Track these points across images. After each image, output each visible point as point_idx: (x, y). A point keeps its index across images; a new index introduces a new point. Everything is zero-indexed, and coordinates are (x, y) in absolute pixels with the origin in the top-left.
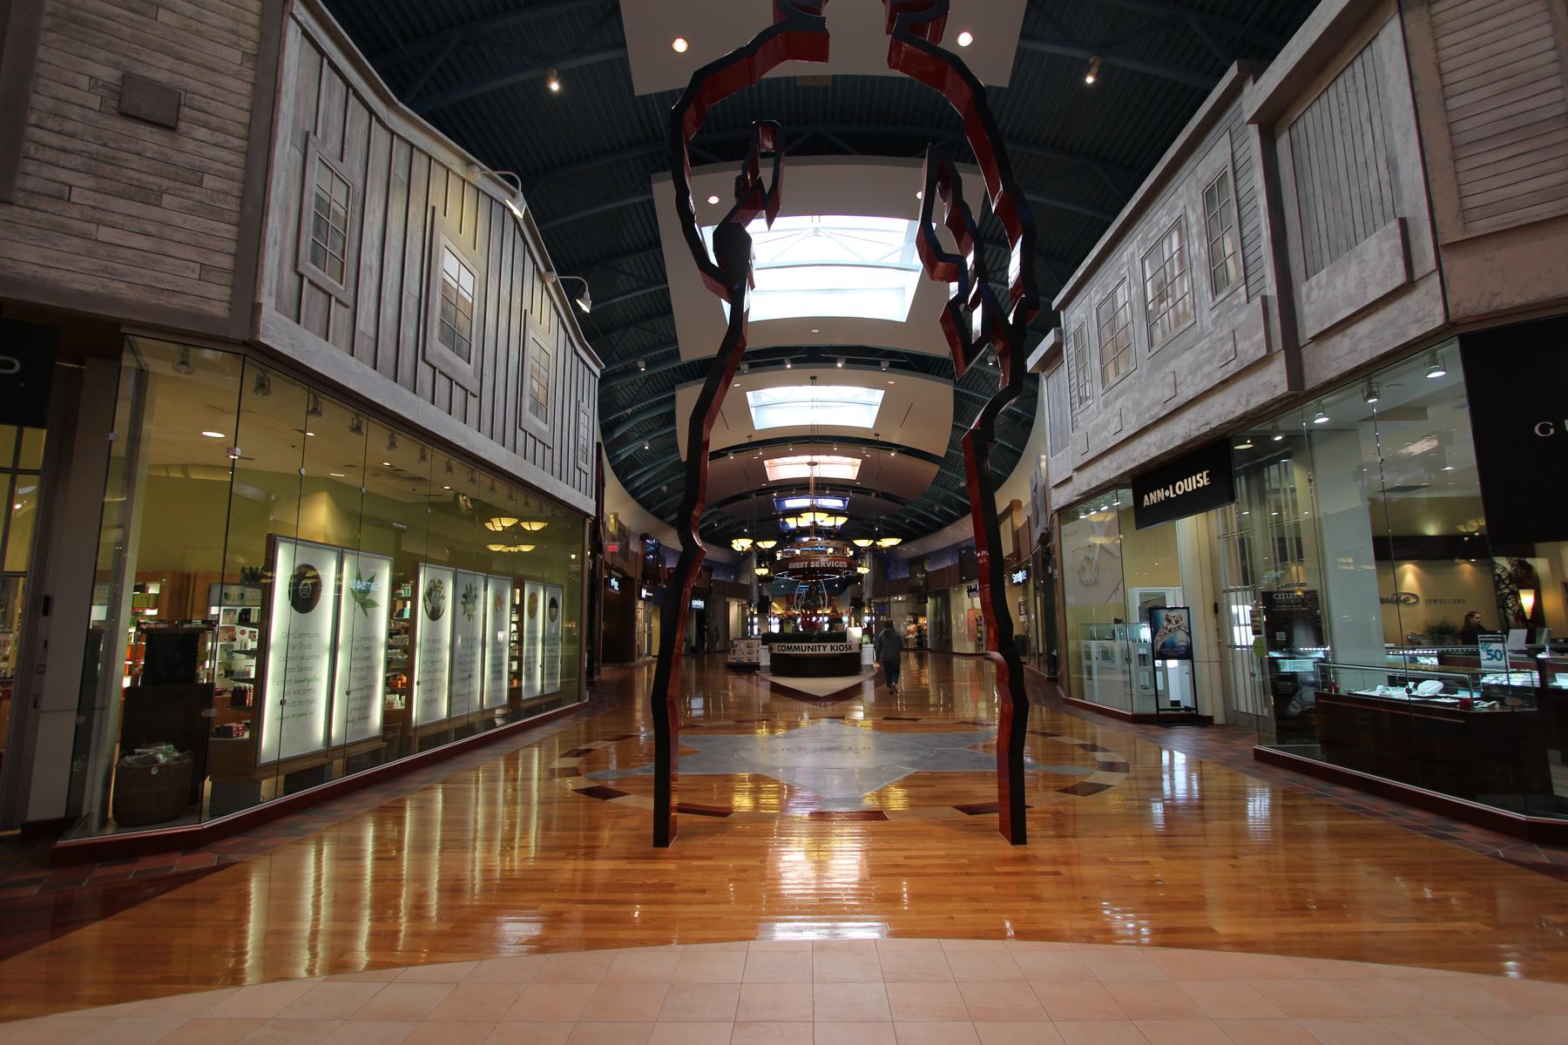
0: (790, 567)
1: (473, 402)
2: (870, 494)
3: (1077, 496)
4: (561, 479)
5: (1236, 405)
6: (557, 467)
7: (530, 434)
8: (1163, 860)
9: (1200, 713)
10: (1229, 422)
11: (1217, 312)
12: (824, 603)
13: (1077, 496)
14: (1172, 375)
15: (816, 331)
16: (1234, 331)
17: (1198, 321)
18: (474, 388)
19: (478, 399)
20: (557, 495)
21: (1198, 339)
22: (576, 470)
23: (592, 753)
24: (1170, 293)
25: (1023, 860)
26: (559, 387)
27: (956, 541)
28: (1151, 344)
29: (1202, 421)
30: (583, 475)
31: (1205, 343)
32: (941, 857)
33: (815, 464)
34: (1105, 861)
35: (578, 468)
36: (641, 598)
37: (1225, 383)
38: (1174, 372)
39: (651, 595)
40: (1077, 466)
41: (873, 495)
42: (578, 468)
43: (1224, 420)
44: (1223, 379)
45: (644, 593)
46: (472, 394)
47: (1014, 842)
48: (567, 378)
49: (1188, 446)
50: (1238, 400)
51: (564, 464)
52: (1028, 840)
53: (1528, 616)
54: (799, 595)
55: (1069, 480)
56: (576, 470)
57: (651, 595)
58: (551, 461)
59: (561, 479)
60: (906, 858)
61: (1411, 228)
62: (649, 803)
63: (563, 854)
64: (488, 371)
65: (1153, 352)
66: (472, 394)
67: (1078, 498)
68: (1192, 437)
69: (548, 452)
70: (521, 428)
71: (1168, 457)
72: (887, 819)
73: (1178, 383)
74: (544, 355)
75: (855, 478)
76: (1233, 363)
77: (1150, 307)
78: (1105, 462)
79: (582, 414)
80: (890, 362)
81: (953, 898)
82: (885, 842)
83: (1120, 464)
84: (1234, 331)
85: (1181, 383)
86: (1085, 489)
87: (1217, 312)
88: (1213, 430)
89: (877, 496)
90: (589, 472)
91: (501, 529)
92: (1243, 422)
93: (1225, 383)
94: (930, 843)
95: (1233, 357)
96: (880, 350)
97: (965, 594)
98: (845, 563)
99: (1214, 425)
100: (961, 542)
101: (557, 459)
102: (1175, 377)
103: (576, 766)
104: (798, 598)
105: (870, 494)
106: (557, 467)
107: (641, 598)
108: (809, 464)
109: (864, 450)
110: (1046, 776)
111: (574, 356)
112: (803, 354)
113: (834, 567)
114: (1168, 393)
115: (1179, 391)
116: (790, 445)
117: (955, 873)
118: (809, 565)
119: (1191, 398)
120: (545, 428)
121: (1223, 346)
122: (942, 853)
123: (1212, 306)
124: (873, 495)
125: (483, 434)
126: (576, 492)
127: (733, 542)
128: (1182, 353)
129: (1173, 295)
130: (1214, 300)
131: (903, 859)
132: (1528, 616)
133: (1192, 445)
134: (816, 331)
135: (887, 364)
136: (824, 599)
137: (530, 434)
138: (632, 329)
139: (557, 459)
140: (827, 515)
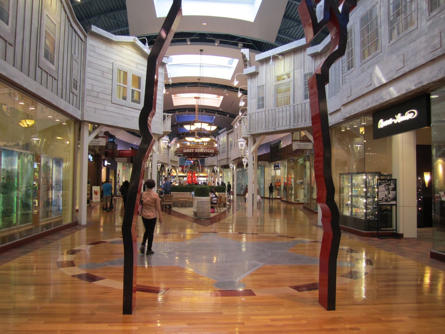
0: (184, 151)
1: (10, 49)
2: (226, 115)
3: (343, 119)
4: (62, 98)
5: (438, 73)
6: (60, 91)
7: (44, 71)
8: (409, 319)
9: (398, 232)
10: (433, 82)
11: (431, 22)
12: (200, 170)
13: (343, 119)
14: (402, 56)
15: (205, 24)
16: (441, 33)
17: (419, 26)
18: (11, 40)
19: (13, 47)
20: (60, 107)
21: (418, 37)
22: (71, 93)
23: (82, 252)
24: (403, 11)
25: (333, 321)
26: (62, 45)
27: (269, 141)
28: (391, 38)
29: (418, 81)
30: (75, 97)
31: (423, 39)
32: (291, 319)
33: (199, 98)
34: (379, 320)
35: (72, 92)
36: (104, 166)
37: (433, 61)
38: (403, 54)
39: (110, 164)
40: (344, 104)
41: (228, 116)
42: (72, 92)
43: (430, 81)
44: (432, 59)
45: (106, 163)
46: (10, 44)
47: (329, 309)
48: (66, 40)
49: (406, 95)
50: (439, 70)
51: (64, 90)
52: (336, 307)
53: (427, 186)
54: (187, 166)
55: (339, 110)
56: (71, 93)
57: (110, 164)
58: (56, 87)
59: (62, 98)
60: (272, 320)
61: (236, 92)
62: (119, 285)
63: (68, 319)
64: (19, 31)
65: (391, 44)
66: (10, 44)
67: (343, 120)
68: (412, 89)
69: (55, 82)
70: (39, 67)
71: (395, 100)
72: (256, 295)
73: (405, 60)
74: (52, 25)
75: (219, 106)
76: (439, 50)
77: (391, 19)
78: (360, 102)
79: (74, 62)
80: (243, 44)
81: (77, 208)
82: (257, 310)
83: (369, 103)
84: (441, 33)
85: (407, 60)
86: (348, 115)
87: (431, 22)
88: (423, 86)
89: (230, 116)
90: (78, 95)
91: (26, 126)
92: (440, 83)
93: (433, 61)
94: (282, 310)
95: (439, 46)
96: (238, 37)
97: (273, 168)
98: (213, 150)
99: (425, 83)
100: (271, 142)
101: (60, 86)
102: (404, 57)
103: (73, 260)
104: (186, 168)
105: (226, 115)
106: (60, 91)
107: (104, 166)
108: (195, 98)
109: (225, 91)
110: (165, 216)
111: (70, 28)
112: (196, 36)
113: (208, 152)
114: (401, 65)
115: (405, 65)
116: (186, 87)
117: (302, 330)
118: (194, 151)
119: (412, 69)
120: (53, 67)
121: (433, 41)
122: (291, 317)
123: (428, 19)
124: (228, 116)
125: (16, 68)
126: (71, 106)
127: (171, 131)
128: (409, 44)
129: (405, 12)
130: (429, 15)
131: (270, 321)
132: (427, 186)
133: (410, 94)
134: (205, 24)
135: (242, 45)
136: (199, 169)
137: (44, 71)
138: (102, 17)
139: (60, 86)
140: (208, 125)
